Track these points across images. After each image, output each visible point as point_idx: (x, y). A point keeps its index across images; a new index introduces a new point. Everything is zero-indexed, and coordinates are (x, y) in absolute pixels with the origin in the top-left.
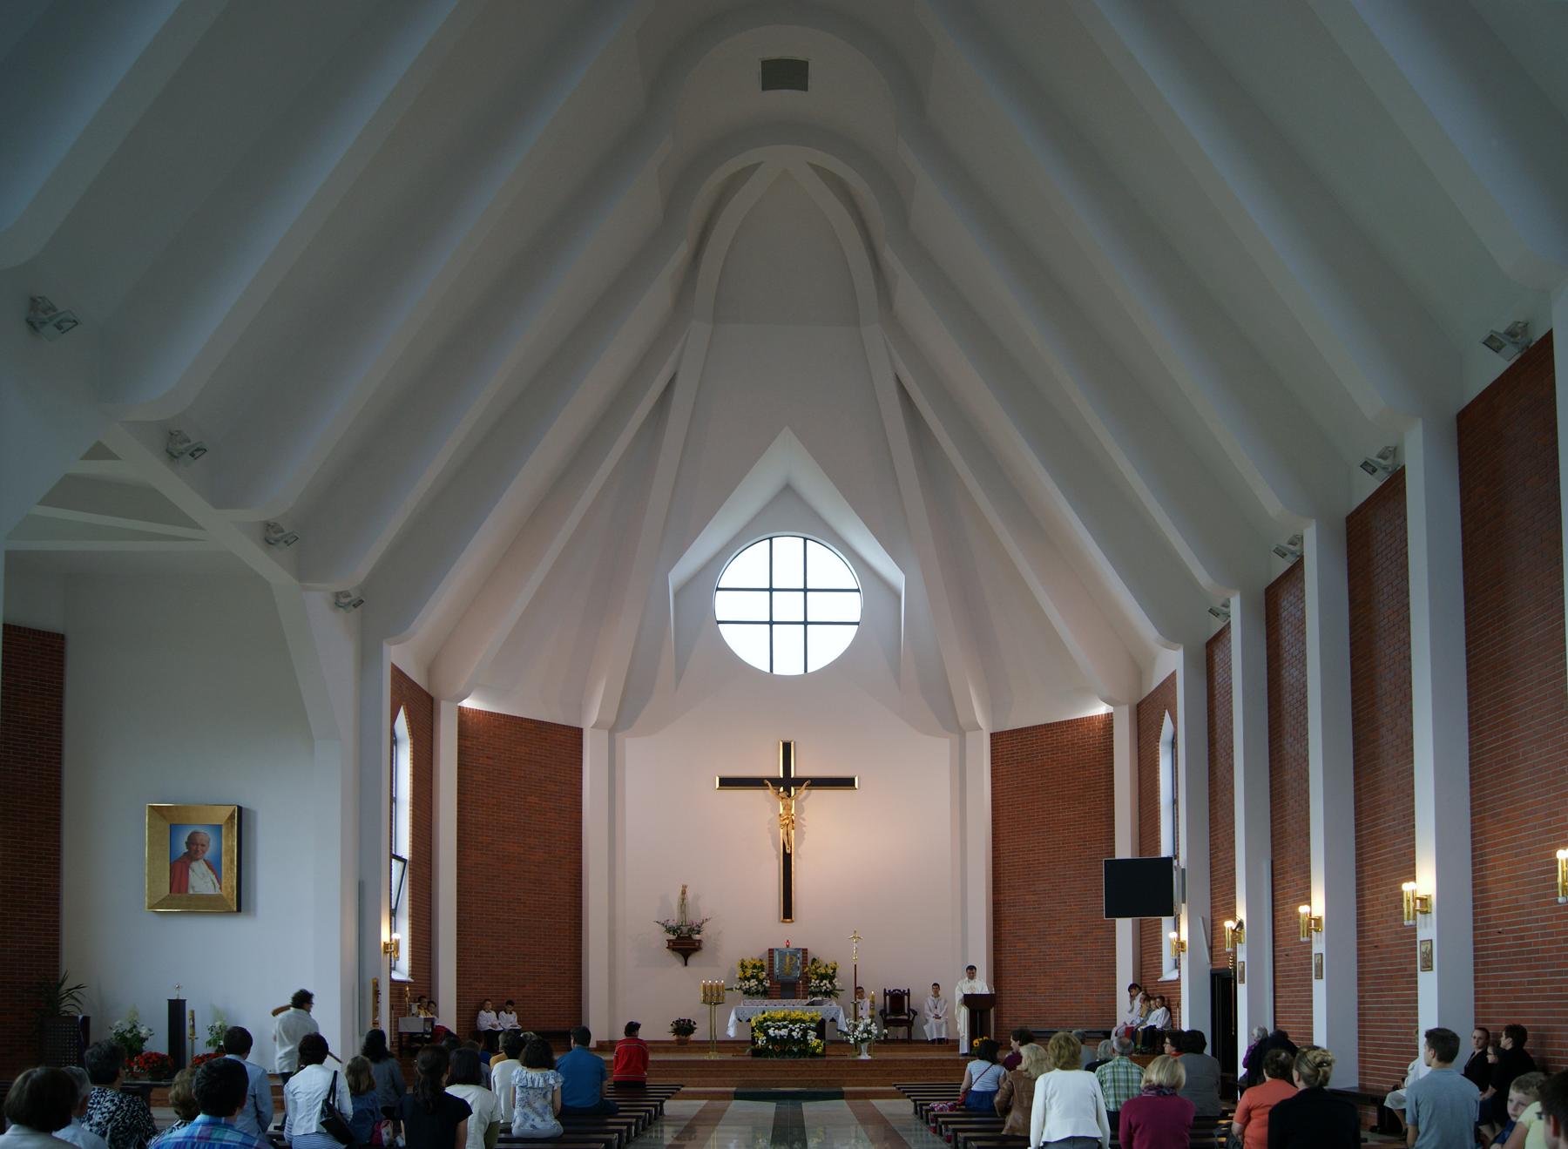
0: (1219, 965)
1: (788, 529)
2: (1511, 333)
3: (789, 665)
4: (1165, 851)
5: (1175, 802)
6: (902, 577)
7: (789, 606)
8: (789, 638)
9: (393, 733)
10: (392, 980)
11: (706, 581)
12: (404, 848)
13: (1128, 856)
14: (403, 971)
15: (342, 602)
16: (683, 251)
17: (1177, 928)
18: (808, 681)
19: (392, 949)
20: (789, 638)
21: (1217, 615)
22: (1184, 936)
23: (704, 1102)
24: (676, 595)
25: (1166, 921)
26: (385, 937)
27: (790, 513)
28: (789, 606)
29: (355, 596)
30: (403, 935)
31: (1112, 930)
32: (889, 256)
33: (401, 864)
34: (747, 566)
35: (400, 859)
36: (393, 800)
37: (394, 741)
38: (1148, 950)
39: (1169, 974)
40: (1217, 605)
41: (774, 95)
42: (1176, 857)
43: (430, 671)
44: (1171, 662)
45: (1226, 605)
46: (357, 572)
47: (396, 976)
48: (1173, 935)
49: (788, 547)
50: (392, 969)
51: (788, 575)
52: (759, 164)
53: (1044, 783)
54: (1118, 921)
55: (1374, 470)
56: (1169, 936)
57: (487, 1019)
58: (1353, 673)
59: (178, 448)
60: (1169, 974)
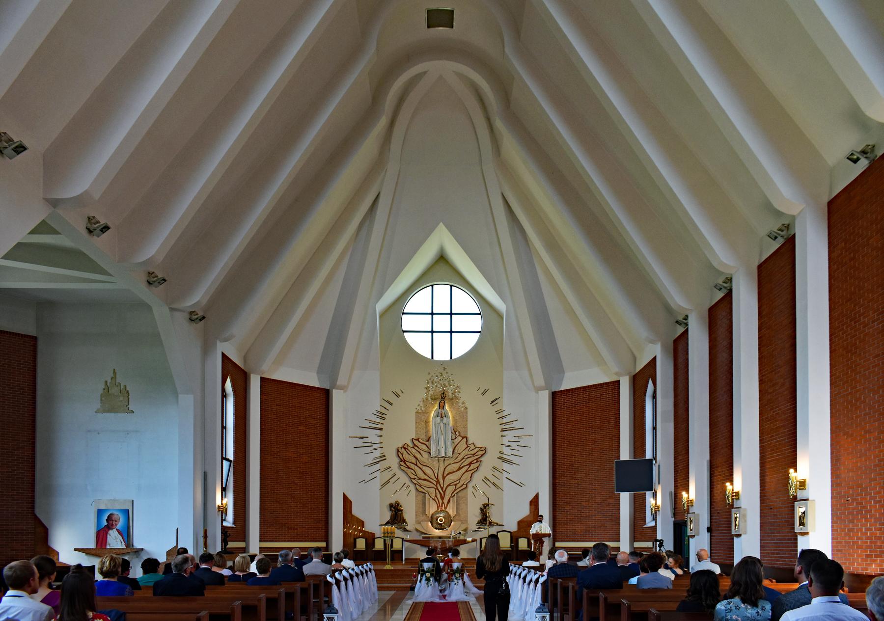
0: (679, 518)
1: (442, 280)
2: (864, 152)
3: (442, 355)
4: (649, 455)
5: (654, 428)
6: (504, 306)
7: (442, 323)
8: (442, 306)
9: (223, 390)
10: (222, 526)
11: (397, 308)
12: (230, 455)
13: (628, 459)
14: (229, 521)
15: (194, 317)
16: (383, 122)
17: (655, 496)
18: (453, 363)
19: (223, 510)
20: (442, 340)
21: (680, 324)
22: (659, 503)
23: (393, 592)
24: (380, 317)
25: (649, 494)
26: (218, 502)
27: (441, 269)
28: (442, 323)
29: (201, 314)
30: (229, 501)
31: (618, 499)
32: (499, 124)
33: (228, 463)
34: (419, 301)
35: (228, 460)
36: (224, 428)
37: (224, 396)
38: (638, 507)
39: (650, 523)
40: (680, 318)
41: (432, 30)
42: (655, 459)
43: (245, 359)
44: (655, 350)
45: (686, 318)
46: (198, 297)
47: (225, 524)
48: (653, 501)
49: (442, 291)
50: (223, 520)
51: (442, 306)
52: (425, 73)
53: (580, 418)
54: (622, 494)
55: (776, 238)
56: (650, 501)
57: (231, 545)
58: (760, 355)
59: (153, 280)
60: (650, 523)
